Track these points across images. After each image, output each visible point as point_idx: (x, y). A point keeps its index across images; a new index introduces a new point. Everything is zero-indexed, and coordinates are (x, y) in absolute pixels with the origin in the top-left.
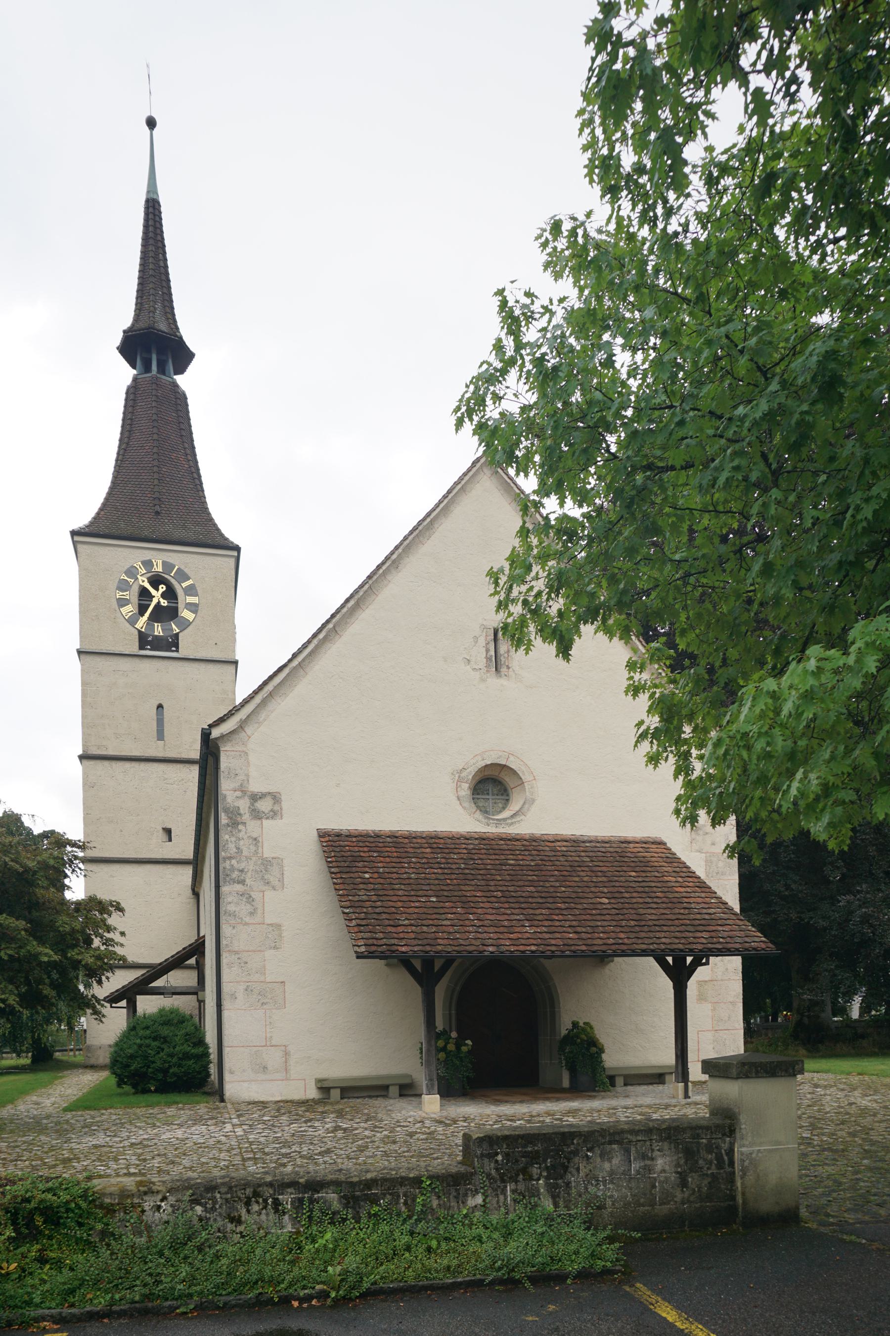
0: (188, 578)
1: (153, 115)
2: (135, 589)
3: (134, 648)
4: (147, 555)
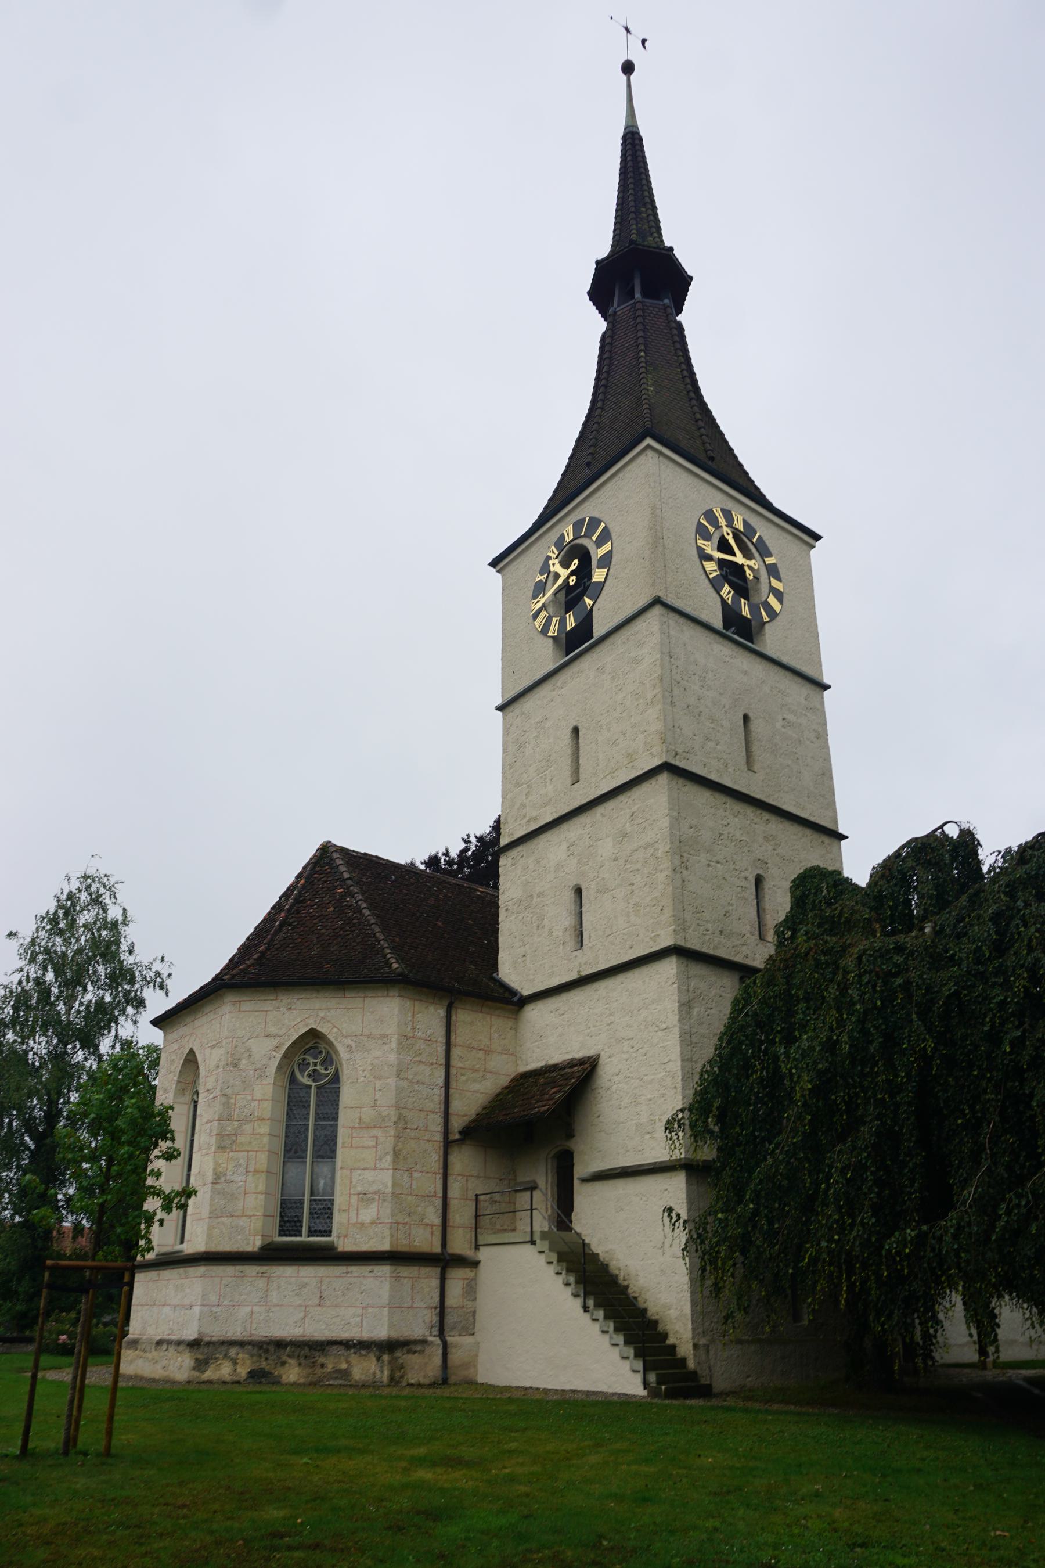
0: (771, 555)
1: (630, 58)
2: (715, 540)
3: (718, 623)
4: (730, 505)
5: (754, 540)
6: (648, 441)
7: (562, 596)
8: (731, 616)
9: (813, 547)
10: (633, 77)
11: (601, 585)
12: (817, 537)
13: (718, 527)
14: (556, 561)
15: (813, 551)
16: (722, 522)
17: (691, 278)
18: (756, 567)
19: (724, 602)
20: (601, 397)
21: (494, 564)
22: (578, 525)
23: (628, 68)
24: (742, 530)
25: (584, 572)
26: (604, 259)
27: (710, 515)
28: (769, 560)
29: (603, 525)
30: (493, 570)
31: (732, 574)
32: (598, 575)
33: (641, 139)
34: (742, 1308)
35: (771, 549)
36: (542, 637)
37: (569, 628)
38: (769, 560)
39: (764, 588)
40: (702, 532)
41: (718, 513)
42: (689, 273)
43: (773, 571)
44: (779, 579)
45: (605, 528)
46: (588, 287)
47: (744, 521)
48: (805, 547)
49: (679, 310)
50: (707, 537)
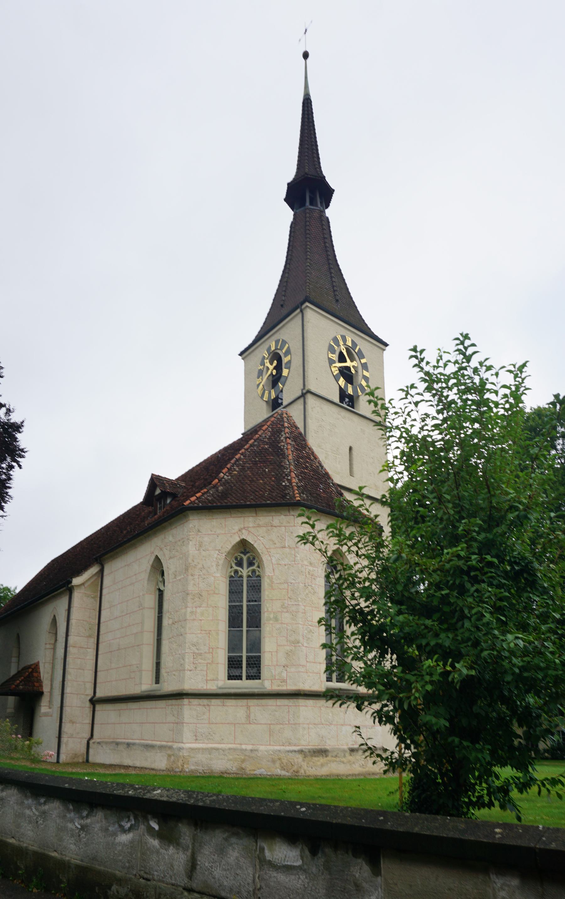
2: (337, 353)
3: (337, 400)
5: (356, 351)
6: (307, 304)
7: (271, 377)
8: (343, 394)
9: (384, 350)
10: (308, 60)
11: (286, 378)
12: (386, 345)
13: (338, 345)
14: (268, 361)
15: (385, 352)
16: (341, 343)
17: (334, 190)
18: (356, 365)
19: (340, 387)
20: (285, 280)
21: (241, 354)
22: (277, 342)
23: (306, 55)
24: (350, 345)
25: (279, 368)
26: (292, 182)
27: (335, 340)
28: (363, 361)
29: (287, 345)
30: (240, 357)
31: (346, 374)
32: (285, 372)
33: (311, 102)
34: (445, 531)
35: (364, 354)
36: (260, 399)
37: (272, 398)
38: (363, 361)
39: (360, 377)
40: (331, 350)
41: (339, 338)
42: (333, 187)
43: (365, 367)
44: (367, 371)
45: (289, 347)
46: (284, 195)
47: (352, 341)
48: (381, 351)
49: (327, 206)
50: (333, 352)
